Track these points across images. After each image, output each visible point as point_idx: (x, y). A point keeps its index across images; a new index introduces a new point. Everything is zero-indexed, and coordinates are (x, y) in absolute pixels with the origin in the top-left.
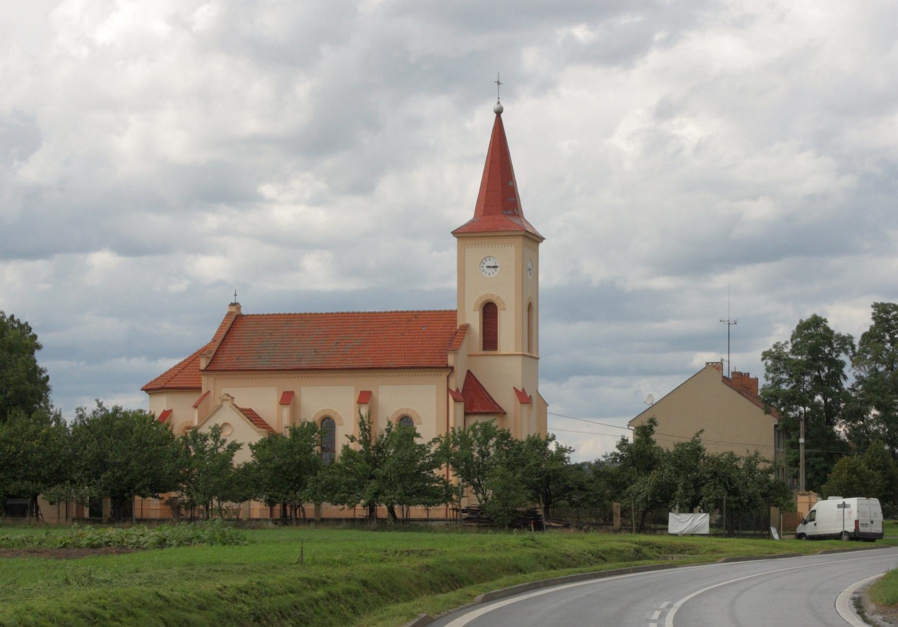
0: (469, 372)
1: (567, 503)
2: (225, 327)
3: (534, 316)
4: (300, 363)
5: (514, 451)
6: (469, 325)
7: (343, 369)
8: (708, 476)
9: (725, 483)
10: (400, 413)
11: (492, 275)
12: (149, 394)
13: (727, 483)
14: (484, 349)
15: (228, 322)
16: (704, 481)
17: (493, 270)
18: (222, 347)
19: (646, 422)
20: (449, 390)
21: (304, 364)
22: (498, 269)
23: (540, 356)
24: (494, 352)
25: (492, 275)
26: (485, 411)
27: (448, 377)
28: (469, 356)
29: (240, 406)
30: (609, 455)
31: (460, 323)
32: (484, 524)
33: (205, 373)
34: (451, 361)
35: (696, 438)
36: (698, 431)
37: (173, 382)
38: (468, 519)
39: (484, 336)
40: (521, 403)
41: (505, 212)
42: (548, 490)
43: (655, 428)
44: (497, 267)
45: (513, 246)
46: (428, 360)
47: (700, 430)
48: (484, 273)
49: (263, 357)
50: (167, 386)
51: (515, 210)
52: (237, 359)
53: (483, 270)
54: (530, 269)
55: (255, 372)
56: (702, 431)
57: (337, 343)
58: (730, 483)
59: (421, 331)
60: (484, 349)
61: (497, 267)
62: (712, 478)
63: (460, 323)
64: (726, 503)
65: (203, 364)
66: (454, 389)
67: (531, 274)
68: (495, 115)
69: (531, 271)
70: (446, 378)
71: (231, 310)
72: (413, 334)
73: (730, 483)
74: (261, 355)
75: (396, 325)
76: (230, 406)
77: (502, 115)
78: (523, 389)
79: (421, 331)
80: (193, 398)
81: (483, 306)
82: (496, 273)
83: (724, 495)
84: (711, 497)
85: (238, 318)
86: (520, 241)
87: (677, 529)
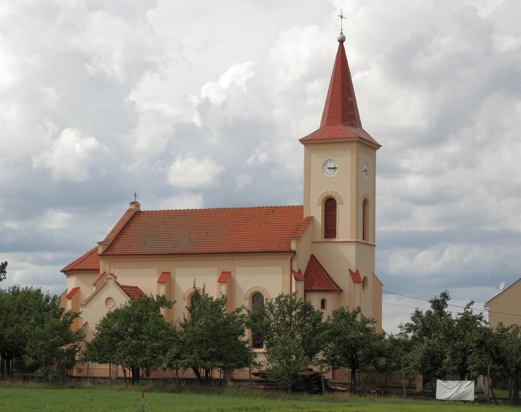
0: (313, 257)
1: (373, 368)
2: (124, 221)
3: (370, 211)
4: (176, 248)
5: (313, 321)
6: (313, 217)
7: (192, 254)
8: (474, 345)
9: (491, 352)
10: (253, 290)
11: (332, 175)
12: (66, 275)
13: (494, 352)
14: (326, 237)
15: (127, 217)
16: (471, 350)
17: (333, 171)
18: (119, 236)
19: (439, 296)
20: (292, 271)
21: (178, 250)
22: (337, 170)
23: (376, 243)
24: (334, 240)
25: (332, 175)
26: (321, 289)
27: (291, 260)
28: (313, 242)
29: (122, 283)
30: (404, 325)
31: (306, 215)
32: (270, 387)
33: (101, 257)
34: (293, 246)
35: (467, 309)
36: (469, 302)
37: (81, 265)
38: (259, 382)
39: (325, 226)
40: (354, 282)
41: (344, 123)
42: (354, 355)
43: (448, 302)
44: (336, 168)
45: (349, 150)
46: (276, 246)
47: (470, 301)
48: (325, 173)
49: (148, 244)
50: (75, 268)
51: (353, 121)
52: (129, 246)
53: (325, 171)
54: (366, 171)
55: (130, 257)
56: (472, 303)
57: (207, 233)
58: (498, 352)
59: (276, 222)
60: (326, 237)
61: (336, 168)
62: (478, 347)
63: (306, 215)
64: (490, 372)
65: (100, 251)
66: (296, 270)
67: (367, 174)
68: (339, 43)
69: (367, 172)
70: (290, 260)
71: (131, 208)
72: (268, 225)
73: (498, 352)
74: (147, 242)
75: (256, 218)
76: (113, 283)
77: (345, 44)
78: (357, 271)
79: (276, 222)
80: (93, 278)
81: (325, 201)
82: (335, 173)
83: (489, 364)
84: (476, 365)
85: (136, 214)
86: (355, 146)
87: (444, 396)
